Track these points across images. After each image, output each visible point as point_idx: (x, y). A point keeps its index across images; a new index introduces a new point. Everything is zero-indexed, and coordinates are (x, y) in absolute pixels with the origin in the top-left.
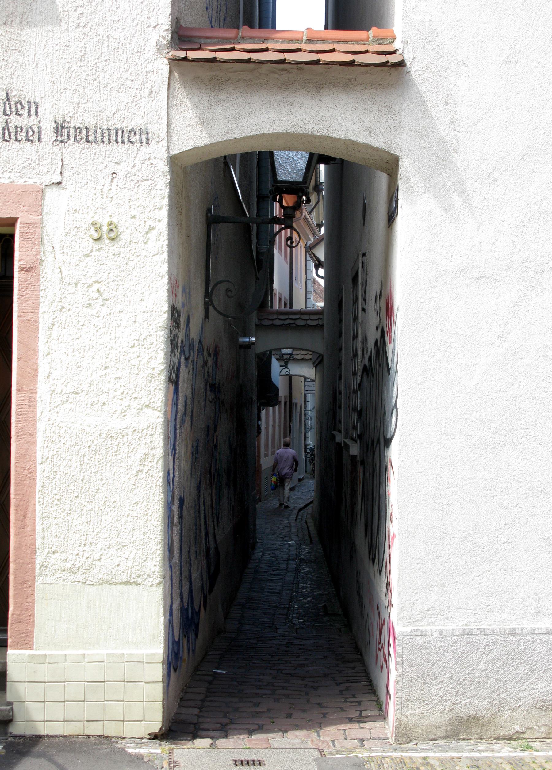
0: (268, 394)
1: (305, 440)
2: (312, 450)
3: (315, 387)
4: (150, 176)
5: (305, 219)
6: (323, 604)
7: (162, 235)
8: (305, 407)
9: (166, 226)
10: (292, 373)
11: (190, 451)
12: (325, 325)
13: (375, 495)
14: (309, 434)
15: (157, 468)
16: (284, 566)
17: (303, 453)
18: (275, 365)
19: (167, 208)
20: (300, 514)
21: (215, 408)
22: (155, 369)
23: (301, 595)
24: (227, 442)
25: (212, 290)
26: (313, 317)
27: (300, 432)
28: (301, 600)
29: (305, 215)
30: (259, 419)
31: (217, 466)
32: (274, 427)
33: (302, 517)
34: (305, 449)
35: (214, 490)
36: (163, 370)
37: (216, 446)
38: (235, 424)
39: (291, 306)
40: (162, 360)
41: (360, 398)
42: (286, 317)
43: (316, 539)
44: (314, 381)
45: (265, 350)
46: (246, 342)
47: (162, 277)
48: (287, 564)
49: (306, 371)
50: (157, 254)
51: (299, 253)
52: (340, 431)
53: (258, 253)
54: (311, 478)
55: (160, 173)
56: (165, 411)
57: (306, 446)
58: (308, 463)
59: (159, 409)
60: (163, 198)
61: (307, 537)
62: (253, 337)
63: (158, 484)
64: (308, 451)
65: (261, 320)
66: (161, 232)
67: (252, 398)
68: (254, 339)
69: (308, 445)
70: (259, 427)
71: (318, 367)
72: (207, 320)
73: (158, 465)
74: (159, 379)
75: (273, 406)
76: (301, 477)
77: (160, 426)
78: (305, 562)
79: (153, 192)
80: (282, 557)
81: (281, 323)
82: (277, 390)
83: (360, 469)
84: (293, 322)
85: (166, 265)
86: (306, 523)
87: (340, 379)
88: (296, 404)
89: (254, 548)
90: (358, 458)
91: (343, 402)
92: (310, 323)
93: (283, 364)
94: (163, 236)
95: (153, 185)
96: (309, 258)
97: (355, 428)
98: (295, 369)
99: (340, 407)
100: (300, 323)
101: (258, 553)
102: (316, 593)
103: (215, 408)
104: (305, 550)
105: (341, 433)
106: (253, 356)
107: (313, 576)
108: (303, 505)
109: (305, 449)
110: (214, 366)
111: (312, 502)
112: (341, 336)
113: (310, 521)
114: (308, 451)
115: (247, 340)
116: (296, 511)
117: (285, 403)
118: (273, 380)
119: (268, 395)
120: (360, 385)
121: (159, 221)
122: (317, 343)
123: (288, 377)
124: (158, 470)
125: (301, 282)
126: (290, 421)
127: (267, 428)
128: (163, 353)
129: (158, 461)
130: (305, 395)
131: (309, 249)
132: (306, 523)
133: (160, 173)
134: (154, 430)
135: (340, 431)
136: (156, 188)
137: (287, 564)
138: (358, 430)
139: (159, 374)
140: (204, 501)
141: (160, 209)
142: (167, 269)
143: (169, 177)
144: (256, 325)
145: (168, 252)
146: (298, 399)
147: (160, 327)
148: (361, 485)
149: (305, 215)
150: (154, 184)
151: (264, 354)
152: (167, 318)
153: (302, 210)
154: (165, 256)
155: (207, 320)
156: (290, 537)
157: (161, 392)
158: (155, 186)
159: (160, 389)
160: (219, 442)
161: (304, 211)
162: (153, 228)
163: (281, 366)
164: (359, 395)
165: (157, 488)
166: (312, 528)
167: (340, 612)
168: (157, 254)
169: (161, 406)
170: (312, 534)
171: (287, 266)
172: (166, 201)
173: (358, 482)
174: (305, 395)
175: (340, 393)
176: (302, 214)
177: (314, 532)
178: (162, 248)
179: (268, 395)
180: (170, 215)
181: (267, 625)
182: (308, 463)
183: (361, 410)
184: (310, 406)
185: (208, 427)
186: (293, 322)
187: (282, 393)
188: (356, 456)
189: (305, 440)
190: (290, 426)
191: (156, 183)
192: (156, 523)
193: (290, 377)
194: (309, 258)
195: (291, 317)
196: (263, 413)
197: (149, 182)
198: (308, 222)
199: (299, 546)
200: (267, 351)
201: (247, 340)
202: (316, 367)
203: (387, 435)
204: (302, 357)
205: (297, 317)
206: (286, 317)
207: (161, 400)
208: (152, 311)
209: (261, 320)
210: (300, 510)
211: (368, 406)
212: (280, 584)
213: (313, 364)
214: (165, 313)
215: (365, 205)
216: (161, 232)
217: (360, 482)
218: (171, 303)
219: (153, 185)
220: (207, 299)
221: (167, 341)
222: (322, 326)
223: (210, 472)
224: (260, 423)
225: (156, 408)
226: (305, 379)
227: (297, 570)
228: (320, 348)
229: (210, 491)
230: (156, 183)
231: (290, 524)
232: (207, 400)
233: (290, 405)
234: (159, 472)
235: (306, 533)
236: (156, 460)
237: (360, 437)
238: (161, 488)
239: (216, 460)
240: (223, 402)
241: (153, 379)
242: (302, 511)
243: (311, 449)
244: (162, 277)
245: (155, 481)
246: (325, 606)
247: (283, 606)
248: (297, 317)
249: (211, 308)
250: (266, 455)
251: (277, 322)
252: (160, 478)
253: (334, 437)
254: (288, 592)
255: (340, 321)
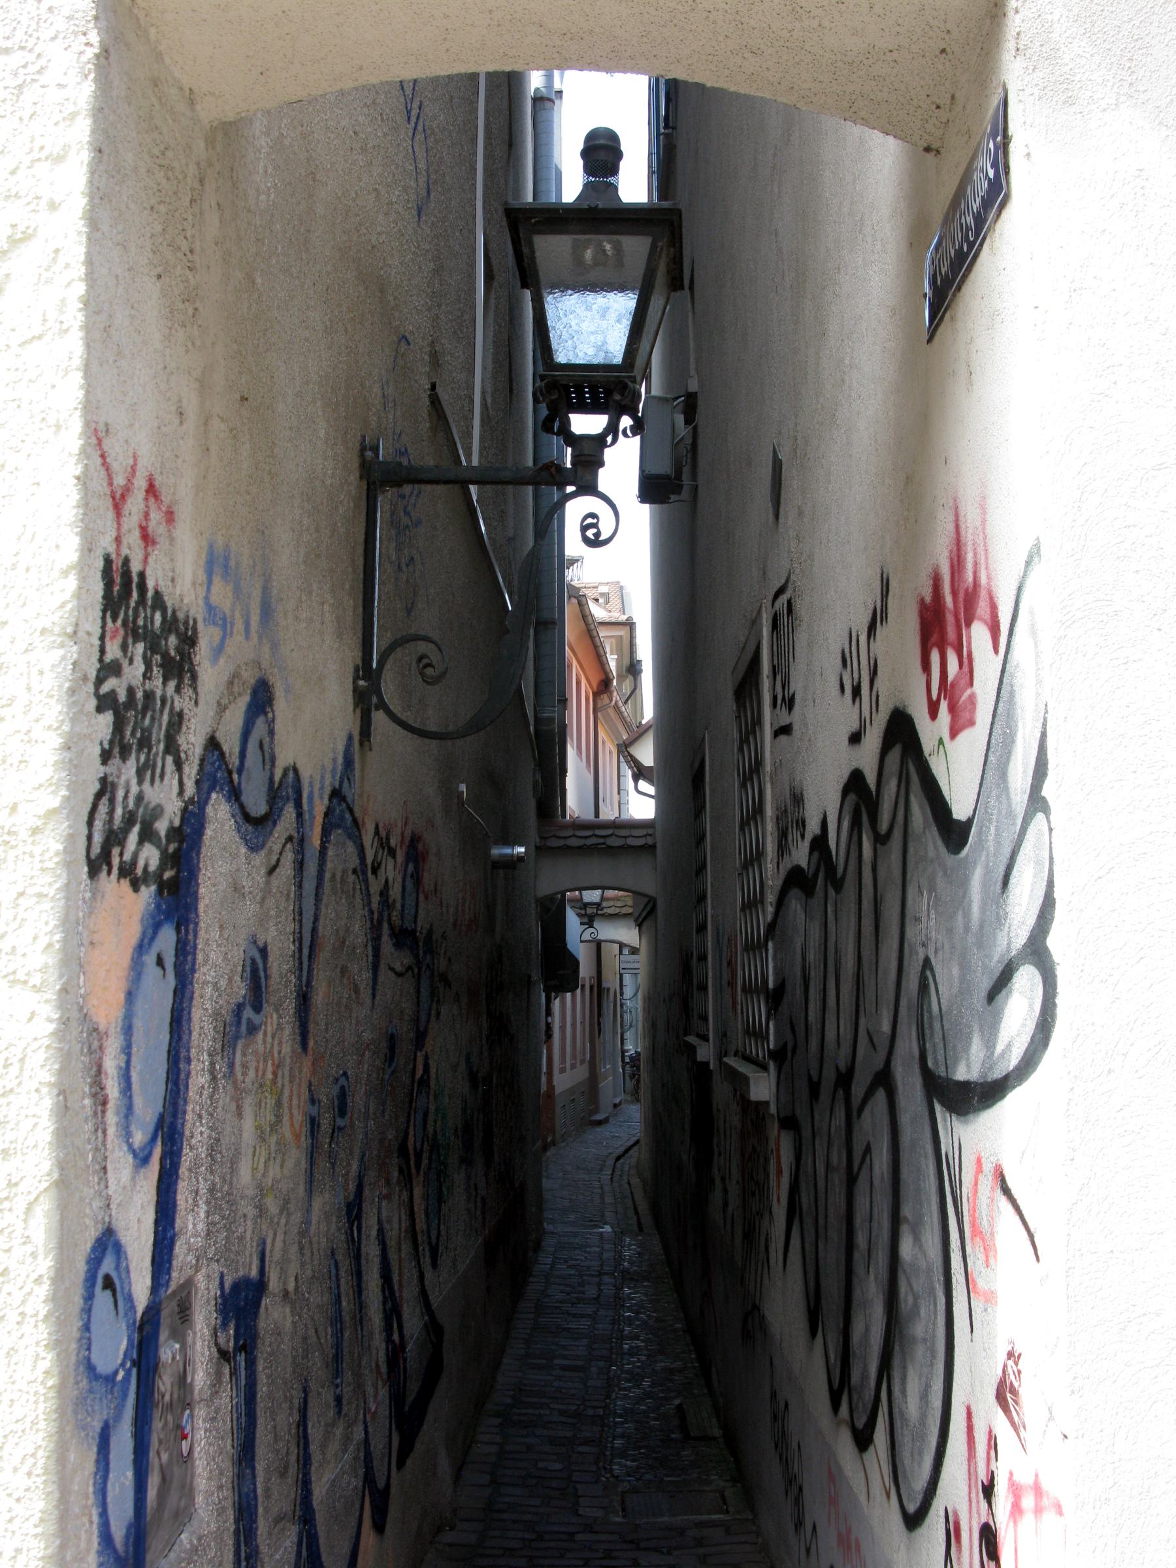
0: (559, 970)
1: (622, 1043)
2: (635, 1059)
3: (641, 962)
4: (20, 35)
5: (616, 708)
6: (677, 1402)
7: (62, 259)
8: (622, 994)
9: (81, 226)
10: (600, 937)
11: (298, 1118)
12: (658, 845)
13: (861, 1239)
14: (628, 1035)
15: (27, 1240)
16: (592, 1292)
17: (620, 1063)
18: (572, 920)
19: (85, 156)
20: (619, 1164)
21: (418, 992)
22: (21, 808)
23: (627, 1372)
24: (463, 1066)
25: (381, 663)
26: (636, 833)
27: (615, 1033)
28: (628, 1389)
29: (616, 702)
30: (549, 1012)
31: (430, 1129)
32: (574, 1025)
33: (622, 1170)
34: (623, 1057)
35: (418, 1192)
36: (53, 812)
37: (424, 1082)
38: (485, 1025)
39: (597, 814)
40: (50, 771)
41: (774, 959)
42: (589, 833)
43: (647, 1221)
44: (634, 951)
45: (551, 892)
46: (506, 855)
47: (58, 427)
48: (599, 1284)
49: (628, 934)
50: (40, 337)
51: (608, 749)
52: (705, 1038)
53: (536, 718)
54: (632, 1102)
55: (60, 24)
56: (64, 990)
57: (623, 1052)
58: (627, 1078)
59: (36, 979)
60: (73, 116)
61: (631, 1213)
62: (521, 845)
63: (29, 1310)
64: (627, 1060)
65: (545, 838)
66: (57, 251)
67: (529, 977)
68: (522, 850)
69: (627, 1051)
70: (549, 1027)
71: (644, 927)
72: (366, 743)
73: (32, 1223)
74: (37, 850)
75: (573, 990)
76: (617, 1101)
77: (42, 1055)
78: (632, 1279)
79: (29, 95)
80: (589, 1268)
81: (580, 842)
82: (576, 963)
83: (784, 1148)
84: (601, 841)
85: (77, 378)
86: (629, 1183)
87: (702, 928)
88: (608, 990)
89: (537, 1247)
90: (773, 1109)
91: (710, 974)
92: (630, 841)
93: (586, 920)
94: (67, 266)
95: (32, 69)
96: (622, 759)
97: (759, 1035)
98: (609, 931)
99: (703, 988)
100: (614, 842)
101: (545, 1260)
102: (659, 1366)
103: (418, 992)
104: (630, 1248)
105: (707, 1040)
106: (533, 901)
107: (649, 1316)
108: (622, 1149)
109: (623, 1057)
110: (409, 884)
111: (637, 1142)
112: (701, 839)
113: (635, 1181)
114: (627, 1060)
115: (508, 851)
116: (610, 1162)
117: (591, 987)
118: (569, 946)
119: (561, 972)
120: (771, 927)
121: (53, 206)
122: (646, 878)
123: (594, 945)
124: (29, 1248)
125: (612, 804)
126: (600, 1015)
127: (563, 1028)
128: (55, 741)
129: (29, 1209)
130: (621, 975)
131: (624, 749)
132: (629, 1183)
133: (60, 24)
134: (14, 1070)
135: (705, 1038)
136: (43, 79)
137: (599, 1284)
138: (771, 1037)
139: (35, 831)
140: (381, 1231)
141: (59, 159)
142: (81, 394)
143: (94, 37)
144: (537, 847)
145: (88, 328)
146: (610, 982)
147: (44, 631)
148: (785, 1180)
149: (616, 702)
150: (37, 67)
151: (551, 898)
152: (78, 595)
153: (611, 693)
154: (73, 346)
155: (366, 743)
156: (603, 1216)
157: (47, 905)
158: (39, 72)
159: (40, 895)
160: (433, 1071)
161: (615, 694)
162: (27, 237)
163: (582, 924)
164: (771, 951)
165: (28, 1328)
166: (639, 1196)
167: (717, 1432)
168: (40, 337)
169: (44, 969)
170: (640, 1209)
171: (591, 778)
172: (82, 131)
173: (772, 1169)
174: (621, 975)
175: (703, 958)
176: (611, 700)
177: (643, 1207)
178: (61, 312)
179: (561, 972)
180: (101, 197)
181: (554, 1484)
182: (627, 1078)
183: (781, 988)
184: (628, 992)
185: (392, 1040)
186: (601, 841)
187: (585, 971)
188: (767, 1103)
189: (622, 1043)
190: (599, 1024)
191: (42, 62)
192: (21, 1482)
193: (598, 944)
194: (622, 759)
195: (598, 832)
196: (556, 1004)
197: (17, 58)
198: (621, 713)
199: (619, 1234)
200: (557, 893)
201: (508, 851)
202: (640, 925)
203: (956, 1063)
204: (618, 910)
205: (609, 832)
206: (589, 833)
207: (43, 941)
208: (14, 567)
209: (545, 838)
210: (618, 1158)
211: (815, 975)
212: (585, 1341)
213: (636, 921)
214: (65, 573)
215: (777, 466)
216: (57, 251)
217: (780, 1172)
218: (106, 543)
219: (32, 69)
220: (361, 683)
221: (72, 691)
222: (653, 847)
223: (403, 1150)
224: (549, 1019)
225: (21, 976)
226: (622, 946)
227: (618, 1301)
228: (649, 883)
229: (405, 1196)
230: (42, 62)
231: (602, 1188)
232: (383, 966)
233: (599, 990)
234: (34, 1255)
235: (630, 1203)
236: (20, 1204)
237: (779, 1056)
238: (42, 1327)
239: (426, 1115)
240: (444, 978)
241: (12, 854)
242: (622, 1161)
243: (631, 1056)
244: (58, 427)
245: (18, 1296)
246: (679, 1408)
247: (590, 1412)
248: (609, 832)
249: (378, 717)
250: (563, 1070)
251: (573, 842)
252: (38, 1281)
253: (692, 1049)
254: (602, 1364)
255: (699, 810)
